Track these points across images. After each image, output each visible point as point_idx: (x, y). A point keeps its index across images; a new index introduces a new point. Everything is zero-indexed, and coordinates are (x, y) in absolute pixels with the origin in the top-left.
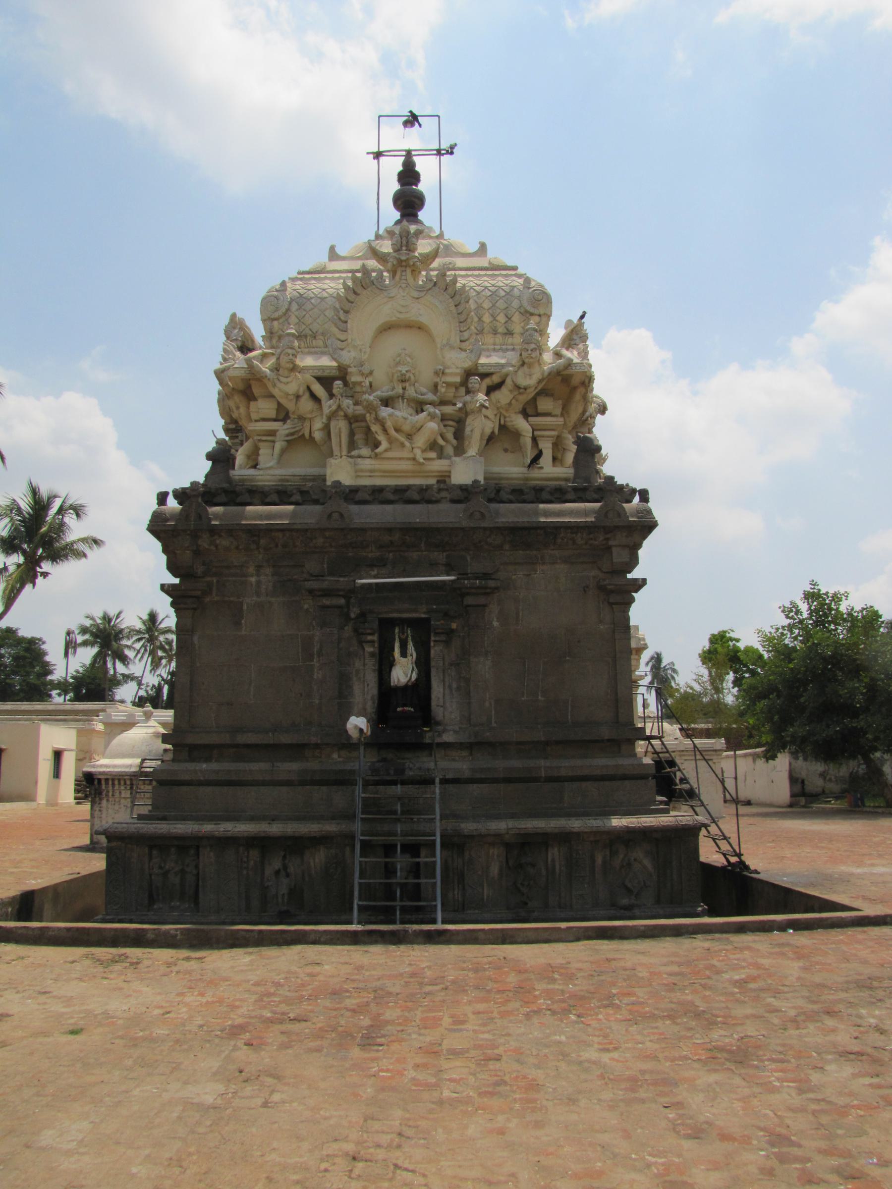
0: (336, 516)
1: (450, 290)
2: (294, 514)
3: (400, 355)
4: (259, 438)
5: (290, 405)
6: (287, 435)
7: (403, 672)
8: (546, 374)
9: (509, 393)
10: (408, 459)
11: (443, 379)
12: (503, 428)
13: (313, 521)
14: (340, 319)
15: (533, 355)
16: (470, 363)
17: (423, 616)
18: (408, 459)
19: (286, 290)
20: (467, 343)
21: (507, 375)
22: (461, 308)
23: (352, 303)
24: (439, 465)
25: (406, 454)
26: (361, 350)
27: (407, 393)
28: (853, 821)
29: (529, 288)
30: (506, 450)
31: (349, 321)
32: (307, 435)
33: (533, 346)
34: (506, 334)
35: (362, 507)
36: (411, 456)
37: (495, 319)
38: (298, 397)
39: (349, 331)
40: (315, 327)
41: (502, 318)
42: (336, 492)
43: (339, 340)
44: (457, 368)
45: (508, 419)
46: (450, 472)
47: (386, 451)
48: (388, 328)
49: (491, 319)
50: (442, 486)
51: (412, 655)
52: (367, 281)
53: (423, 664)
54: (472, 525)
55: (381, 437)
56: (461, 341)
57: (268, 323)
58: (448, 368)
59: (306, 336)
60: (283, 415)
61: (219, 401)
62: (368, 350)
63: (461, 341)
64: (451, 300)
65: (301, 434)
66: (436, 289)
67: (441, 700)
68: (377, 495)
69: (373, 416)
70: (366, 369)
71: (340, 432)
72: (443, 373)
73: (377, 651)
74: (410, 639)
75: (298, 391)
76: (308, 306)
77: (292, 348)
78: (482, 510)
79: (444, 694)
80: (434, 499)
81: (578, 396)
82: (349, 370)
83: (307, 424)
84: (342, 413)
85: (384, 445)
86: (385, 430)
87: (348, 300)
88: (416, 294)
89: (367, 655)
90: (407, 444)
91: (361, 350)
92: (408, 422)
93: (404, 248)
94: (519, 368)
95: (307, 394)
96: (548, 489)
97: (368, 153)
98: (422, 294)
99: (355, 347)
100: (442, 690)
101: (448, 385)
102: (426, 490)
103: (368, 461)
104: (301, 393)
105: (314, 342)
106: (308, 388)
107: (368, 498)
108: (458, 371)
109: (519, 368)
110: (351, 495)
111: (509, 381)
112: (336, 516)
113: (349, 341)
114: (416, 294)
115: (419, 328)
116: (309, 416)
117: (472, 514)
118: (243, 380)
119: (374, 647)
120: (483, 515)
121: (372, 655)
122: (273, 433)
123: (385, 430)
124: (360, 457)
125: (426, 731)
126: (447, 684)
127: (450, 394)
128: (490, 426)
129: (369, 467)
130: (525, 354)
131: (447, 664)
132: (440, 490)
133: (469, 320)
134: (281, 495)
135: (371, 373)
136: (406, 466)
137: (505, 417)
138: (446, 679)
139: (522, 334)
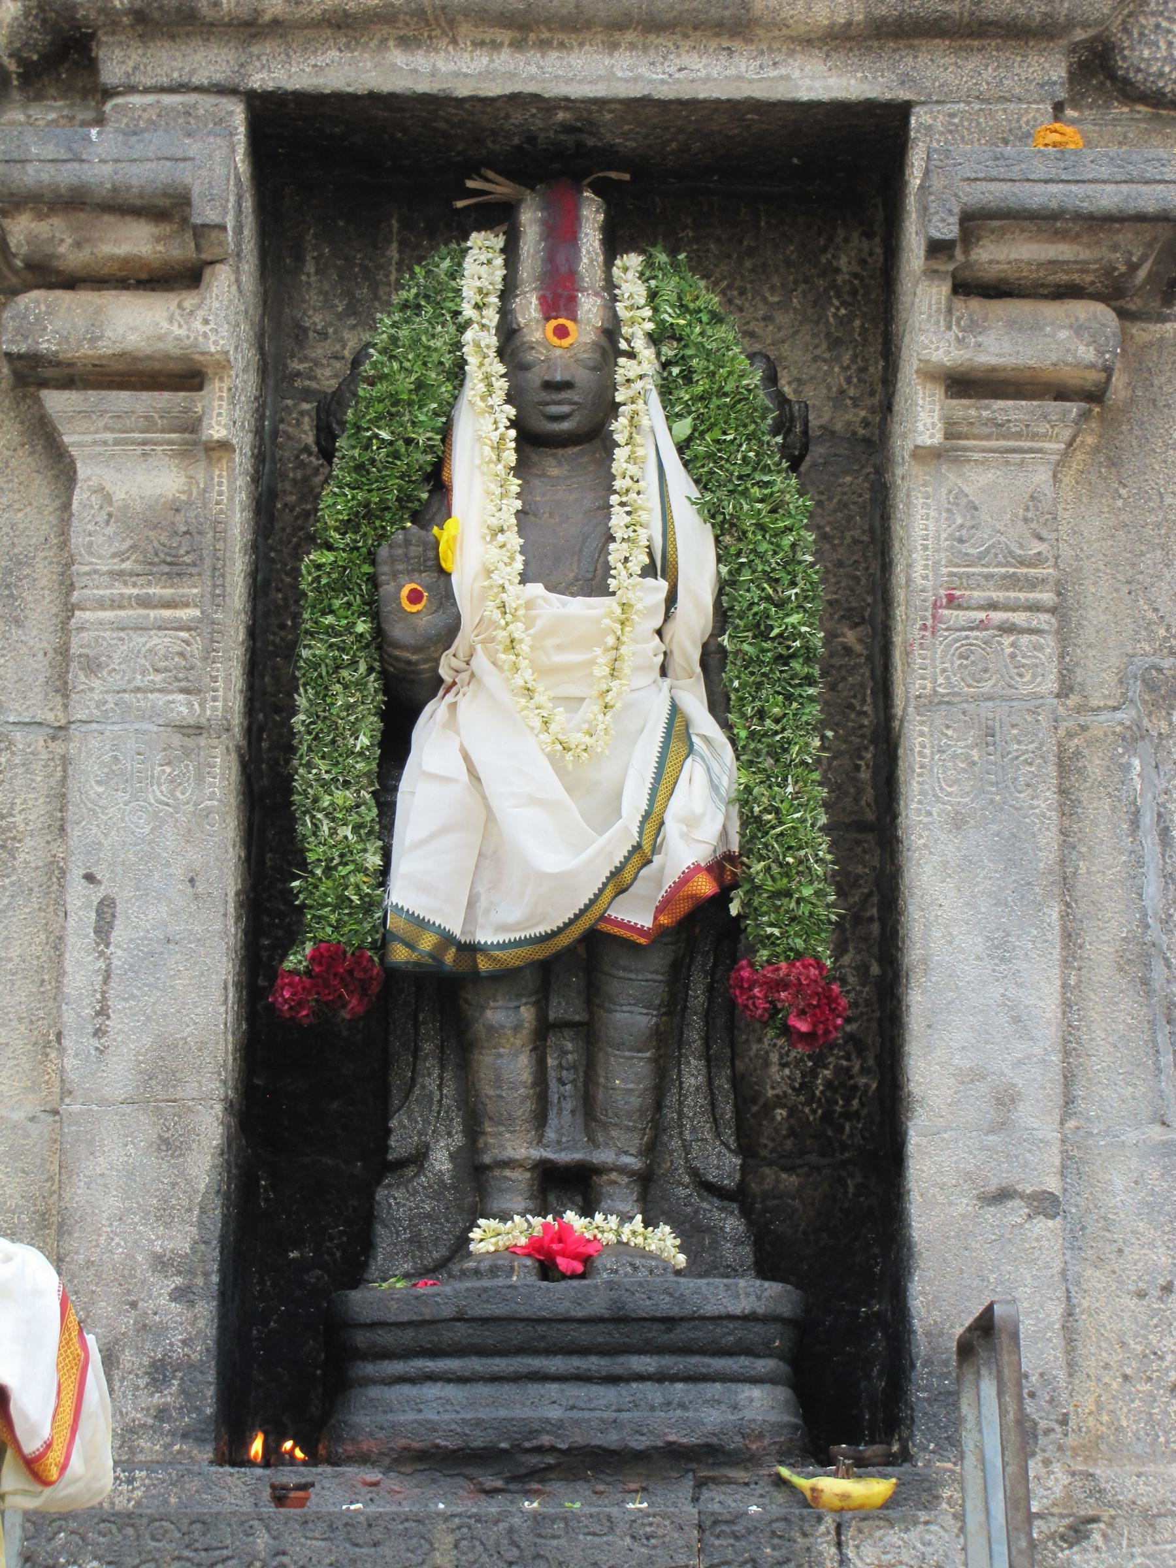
7: (552, 776)
17: (817, 80)
28: (908, 1037)
51: (662, 565)
53: (817, 674)
67: (1038, 1118)
73: (229, 495)
74: (639, 371)
79: (1070, 1047)
89: (98, 546)
100: (1044, 1000)
119: (194, 446)
121: (169, 550)
125: (848, 1518)
126: (1104, 942)
131: (1100, 677)
138: (1102, 868)
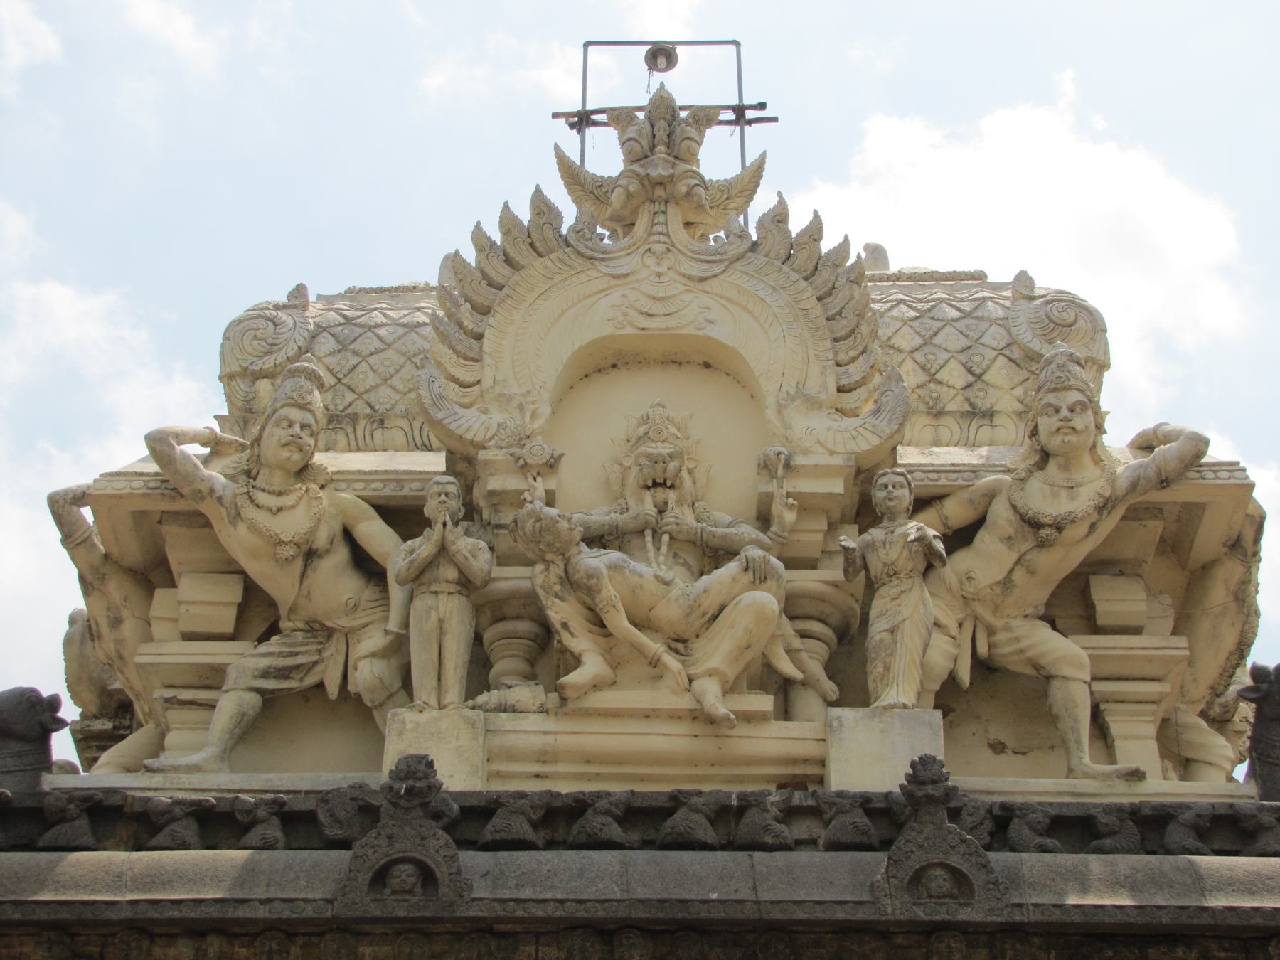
0: (405, 875)
1: (801, 258)
2: (247, 874)
3: (646, 420)
4: (169, 693)
5: (280, 584)
6: (265, 674)
8: (1122, 484)
9: (1001, 547)
10: (674, 716)
11: (789, 486)
12: (984, 667)
13: (318, 895)
14: (460, 325)
15: (1078, 422)
16: (875, 441)
18: (674, 716)
19: (305, 307)
20: (862, 392)
21: (991, 495)
22: (834, 304)
23: (500, 288)
24: (778, 741)
25: (665, 697)
26: (521, 408)
27: (668, 518)
29: (1033, 298)
30: (998, 748)
31: (488, 333)
32: (333, 690)
33: (1074, 396)
34: (964, 415)
35: (504, 855)
36: (685, 702)
37: (933, 379)
38: (311, 555)
39: (487, 360)
40: (384, 398)
41: (954, 375)
42: (410, 791)
43: (455, 380)
44: (832, 453)
45: (1001, 637)
46: (822, 763)
47: (596, 686)
48: (607, 362)
49: (922, 377)
50: (797, 798)
52: (548, 233)
54: (921, 914)
55: (580, 641)
56: (840, 390)
57: (241, 385)
58: (806, 452)
59: (354, 419)
60: (257, 613)
61: (68, 642)
62: (546, 410)
63: (840, 390)
64: (804, 284)
65: (311, 680)
66: (759, 259)
68: (562, 821)
69: (557, 570)
70: (537, 452)
71: (441, 632)
72: (787, 466)
75: (313, 531)
76: (368, 343)
77: (305, 407)
78: (955, 860)
80: (768, 839)
81: (1218, 594)
82: (482, 455)
83: (334, 650)
84: (452, 574)
85: (592, 666)
86: (598, 623)
87: (485, 276)
88: (696, 270)
90: (671, 661)
91: (521, 408)
92: (675, 592)
93: (661, 148)
94: (1030, 473)
95: (341, 554)
96: (1188, 816)
97: (555, 116)
98: (718, 269)
99: (504, 399)
101: (805, 505)
102: (741, 811)
103: (533, 722)
104: (321, 541)
105: (378, 434)
106: (348, 535)
107: (527, 832)
108: (837, 461)
109: (1030, 473)
110: (474, 820)
111: (1000, 512)
112: (405, 875)
113: (487, 382)
114: (696, 270)
115: (707, 365)
116: (344, 622)
117: (917, 878)
118: (140, 516)
120: (958, 877)
122: (213, 677)
123: (598, 623)
124: (503, 708)
127: (811, 536)
128: (950, 655)
129: (537, 741)
130: (1046, 424)
132: (790, 813)
133: (865, 329)
134: (216, 823)
135: (552, 465)
136: (669, 740)
137: (991, 631)
139: (1020, 414)
